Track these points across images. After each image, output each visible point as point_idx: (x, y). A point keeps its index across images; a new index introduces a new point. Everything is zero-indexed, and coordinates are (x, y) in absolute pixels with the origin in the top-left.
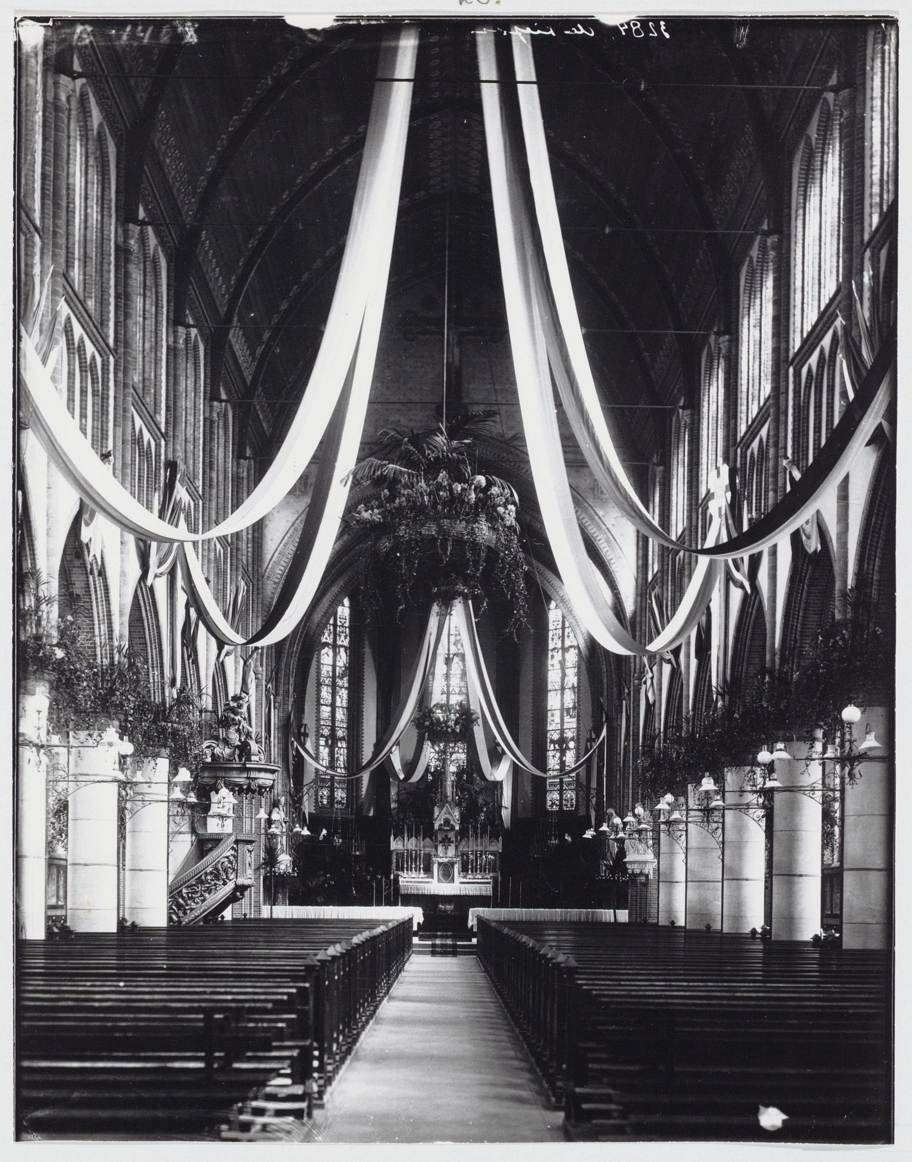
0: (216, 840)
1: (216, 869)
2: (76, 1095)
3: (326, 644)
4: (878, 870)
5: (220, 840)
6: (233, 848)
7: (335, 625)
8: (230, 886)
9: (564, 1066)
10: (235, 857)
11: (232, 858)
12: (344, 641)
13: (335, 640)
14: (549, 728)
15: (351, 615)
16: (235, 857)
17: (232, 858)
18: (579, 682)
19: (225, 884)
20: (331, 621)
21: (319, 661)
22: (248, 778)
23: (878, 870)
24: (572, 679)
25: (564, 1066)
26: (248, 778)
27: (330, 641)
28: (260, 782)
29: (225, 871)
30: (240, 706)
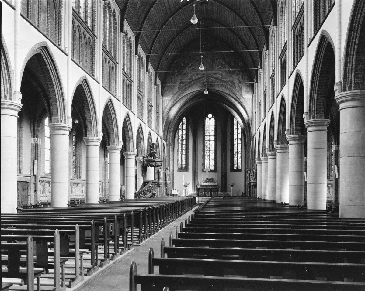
0: (148, 182)
1: (148, 189)
2: (113, 34)
3: (180, 129)
4: (46, 137)
5: (149, 182)
6: (152, 184)
7: (182, 124)
8: (151, 193)
9: (306, 271)
10: (153, 186)
11: (152, 187)
12: (184, 128)
13: (182, 128)
14: (235, 148)
15: (186, 122)
16: (153, 186)
17: (152, 187)
18: (241, 137)
19: (150, 193)
20: (181, 123)
21: (178, 132)
22: (155, 163)
23: (46, 137)
24: (240, 136)
25: (306, 271)
26: (155, 163)
27: (181, 128)
28: (158, 164)
29: (150, 190)
30: (153, 146)
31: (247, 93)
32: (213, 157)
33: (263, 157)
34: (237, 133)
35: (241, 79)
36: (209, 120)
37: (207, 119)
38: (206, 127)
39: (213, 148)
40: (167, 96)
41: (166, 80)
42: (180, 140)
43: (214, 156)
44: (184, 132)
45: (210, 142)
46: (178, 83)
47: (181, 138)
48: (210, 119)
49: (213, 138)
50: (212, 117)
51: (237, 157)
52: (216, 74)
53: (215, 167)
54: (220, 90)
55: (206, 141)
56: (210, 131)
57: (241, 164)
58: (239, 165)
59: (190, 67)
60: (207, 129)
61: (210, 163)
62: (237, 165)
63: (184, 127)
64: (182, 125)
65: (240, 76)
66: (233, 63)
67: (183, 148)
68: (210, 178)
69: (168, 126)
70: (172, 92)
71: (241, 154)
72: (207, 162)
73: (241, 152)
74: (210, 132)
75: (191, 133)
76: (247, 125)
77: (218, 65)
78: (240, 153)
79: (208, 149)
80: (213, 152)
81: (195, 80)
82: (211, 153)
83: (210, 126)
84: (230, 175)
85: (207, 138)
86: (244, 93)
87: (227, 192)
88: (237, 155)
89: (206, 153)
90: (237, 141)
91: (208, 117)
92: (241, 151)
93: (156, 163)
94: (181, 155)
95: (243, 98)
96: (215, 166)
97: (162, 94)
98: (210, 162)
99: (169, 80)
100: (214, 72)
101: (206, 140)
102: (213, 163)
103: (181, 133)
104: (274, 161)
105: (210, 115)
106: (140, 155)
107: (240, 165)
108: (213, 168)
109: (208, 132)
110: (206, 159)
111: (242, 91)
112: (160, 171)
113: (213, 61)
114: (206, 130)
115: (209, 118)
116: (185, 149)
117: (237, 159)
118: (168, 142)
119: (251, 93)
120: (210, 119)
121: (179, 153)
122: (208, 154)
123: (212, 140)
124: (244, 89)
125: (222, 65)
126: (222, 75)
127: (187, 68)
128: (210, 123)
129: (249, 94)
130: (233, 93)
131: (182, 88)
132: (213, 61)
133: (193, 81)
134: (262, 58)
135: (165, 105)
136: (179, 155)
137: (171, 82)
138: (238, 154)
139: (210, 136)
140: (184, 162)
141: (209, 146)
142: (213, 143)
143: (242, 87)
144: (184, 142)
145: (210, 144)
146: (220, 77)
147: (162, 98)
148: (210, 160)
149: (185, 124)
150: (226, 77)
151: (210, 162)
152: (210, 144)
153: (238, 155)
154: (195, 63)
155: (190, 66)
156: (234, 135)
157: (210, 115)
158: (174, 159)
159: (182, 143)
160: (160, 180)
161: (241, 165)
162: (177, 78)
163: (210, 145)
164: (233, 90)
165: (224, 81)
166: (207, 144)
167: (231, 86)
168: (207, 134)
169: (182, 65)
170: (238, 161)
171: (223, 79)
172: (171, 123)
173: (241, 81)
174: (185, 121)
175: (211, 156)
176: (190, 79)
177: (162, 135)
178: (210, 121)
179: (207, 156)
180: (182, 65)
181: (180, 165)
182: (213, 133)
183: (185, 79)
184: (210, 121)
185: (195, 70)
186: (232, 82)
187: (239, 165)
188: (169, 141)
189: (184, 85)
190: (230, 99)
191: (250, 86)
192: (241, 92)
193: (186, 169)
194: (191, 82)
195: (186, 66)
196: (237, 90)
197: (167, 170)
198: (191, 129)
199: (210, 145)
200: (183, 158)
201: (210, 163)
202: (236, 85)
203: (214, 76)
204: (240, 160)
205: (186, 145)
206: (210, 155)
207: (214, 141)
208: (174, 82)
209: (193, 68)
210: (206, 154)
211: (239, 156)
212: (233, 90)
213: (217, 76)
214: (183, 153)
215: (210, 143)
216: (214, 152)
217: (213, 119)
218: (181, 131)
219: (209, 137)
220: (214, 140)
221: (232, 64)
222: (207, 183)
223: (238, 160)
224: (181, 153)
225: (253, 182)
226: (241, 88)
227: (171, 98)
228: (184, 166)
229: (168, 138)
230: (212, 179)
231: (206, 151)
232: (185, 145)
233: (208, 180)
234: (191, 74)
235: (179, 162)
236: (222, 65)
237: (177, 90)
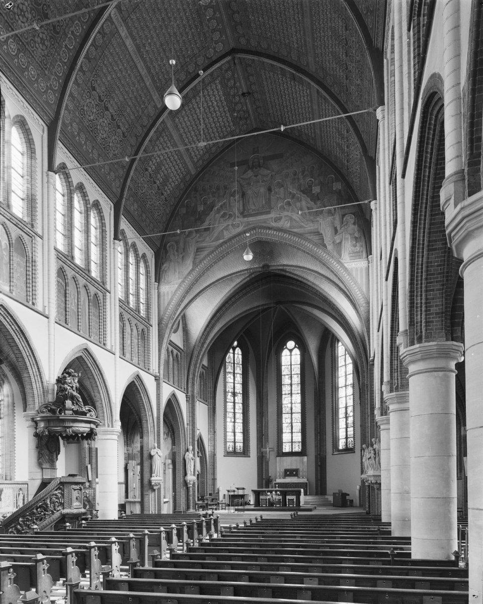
3: (230, 373)
11: (59, 495)
13: (234, 371)
27: (232, 371)
31: (356, 255)
32: (298, 426)
33: (391, 391)
34: (344, 374)
35: (337, 224)
36: (288, 353)
37: (285, 353)
38: (283, 368)
39: (297, 408)
40: (169, 283)
41: (165, 246)
42: (230, 394)
43: (300, 424)
44: (239, 379)
45: (291, 396)
46: (192, 250)
47: (231, 390)
48: (291, 351)
49: (297, 389)
50: (295, 347)
51: (347, 424)
52: (277, 219)
53: (302, 446)
54: (291, 263)
55: (283, 396)
56: (291, 375)
57: (354, 437)
58: (350, 440)
59: (218, 211)
60: (285, 371)
61: (292, 439)
62: (347, 440)
63: (238, 368)
64: (234, 366)
65: (337, 217)
66: (319, 187)
67: (236, 411)
68: (294, 467)
69: (189, 360)
70: (179, 273)
71: (354, 416)
72: (286, 437)
73: (354, 412)
74: (291, 377)
75: (253, 378)
76: (358, 339)
77: (282, 197)
78: (351, 414)
79: (288, 410)
80: (297, 417)
81: (230, 239)
82: (293, 419)
83: (291, 365)
84: (332, 462)
85: (285, 389)
86: (346, 258)
87: (326, 497)
88: (345, 419)
89: (284, 420)
90: (346, 391)
91: (286, 348)
92: (354, 410)
93: (67, 425)
94: (232, 424)
95: (346, 269)
96: (302, 444)
97: (158, 279)
98: (292, 437)
99: (172, 245)
100: (273, 215)
101: (283, 393)
102: (298, 437)
103: (232, 381)
104: (462, 255)
105: (291, 344)
106: (32, 406)
107: (352, 439)
108: (297, 448)
109: (287, 377)
110: (284, 431)
111: (343, 252)
112: (152, 454)
113: (270, 190)
114: (283, 374)
115: (288, 349)
116: (241, 411)
117: (347, 428)
118: (190, 394)
119: (364, 255)
120: (291, 351)
121: (228, 420)
122: (289, 421)
123: (296, 392)
124: (348, 246)
125: (293, 196)
126: (291, 219)
127: (212, 213)
128: (290, 358)
129: (360, 257)
130: (324, 264)
131: (200, 262)
132: (270, 190)
133: (225, 242)
134: (383, 71)
135: (164, 303)
136: (228, 424)
137: (177, 251)
138: (346, 418)
139: (291, 385)
140: (240, 437)
141: (289, 405)
142: (297, 398)
143: (340, 243)
144: (239, 399)
145: (291, 400)
146: (287, 225)
147: (158, 289)
148: (292, 433)
149: (241, 363)
150: (303, 224)
151: (292, 437)
152: (291, 400)
153: (347, 420)
154: (229, 201)
155: (217, 209)
156: (340, 379)
157: (291, 344)
158: (215, 432)
159: (234, 400)
160: (153, 475)
161: (354, 439)
162: (188, 238)
163: (291, 403)
164: (320, 252)
165: (296, 234)
166: (286, 401)
167: (315, 245)
168: (286, 380)
169: (201, 208)
170: (345, 429)
171: (295, 230)
172: (196, 353)
173: (338, 228)
174: (240, 357)
175: (294, 424)
176: (217, 239)
177: (159, 372)
178: (291, 355)
179: (287, 425)
180: (201, 208)
181: (232, 444)
182: (297, 379)
183: (208, 239)
184: (291, 355)
185: (230, 216)
186: (318, 233)
187: (350, 440)
188: (193, 391)
189: (206, 253)
190: (318, 289)
191: (363, 238)
192: (340, 255)
193: (245, 453)
194: (221, 245)
195: (207, 212)
196: (328, 253)
197: (187, 453)
198: (253, 372)
199: (291, 403)
200: (236, 431)
201: (292, 439)
202: (327, 240)
203: (274, 224)
204: (352, 429)
205: (243, 404)
206: (292, 423)
207: (300, 394)
208: (184, 249)
209: (224, 213)
210: (284, 422)
211: (350, 420)
212: (320, 252)
213: (279, 224)
214: (237, 421)
215: (292, 400)
216: (299, 416)
217: (297, 352)
218: (232, 377)
219: (289, 388)
220: (299, 392)
221: (316, 190)
222: (287, 477)
223: (348, 429)
224: (233, 420)
225: (374, 476)
226: (338, 246)
227: (177, 286)
228: (239, 445)
229: (190, 385)
230: (297, 471)
231: (283, 415)
232: (241, 405)
233: (288, 473)
234: (221, 228)
235: (228, 437)
236: (293, 196)
237: (191, 268)
